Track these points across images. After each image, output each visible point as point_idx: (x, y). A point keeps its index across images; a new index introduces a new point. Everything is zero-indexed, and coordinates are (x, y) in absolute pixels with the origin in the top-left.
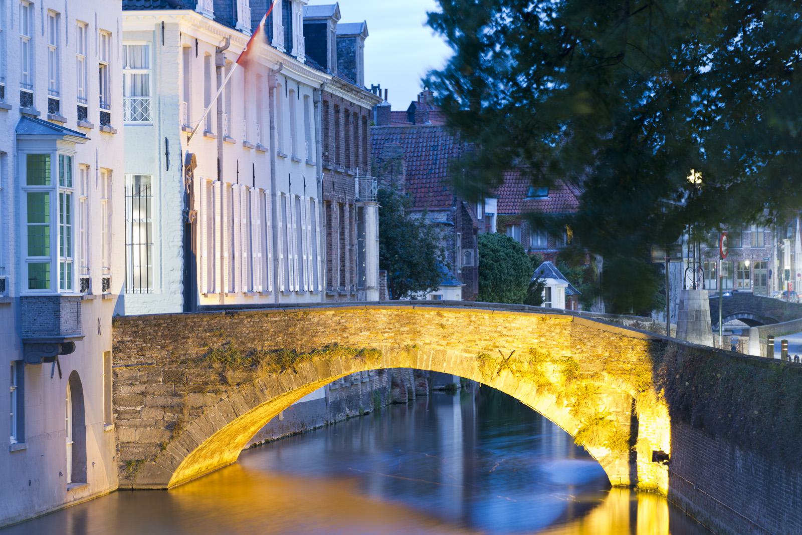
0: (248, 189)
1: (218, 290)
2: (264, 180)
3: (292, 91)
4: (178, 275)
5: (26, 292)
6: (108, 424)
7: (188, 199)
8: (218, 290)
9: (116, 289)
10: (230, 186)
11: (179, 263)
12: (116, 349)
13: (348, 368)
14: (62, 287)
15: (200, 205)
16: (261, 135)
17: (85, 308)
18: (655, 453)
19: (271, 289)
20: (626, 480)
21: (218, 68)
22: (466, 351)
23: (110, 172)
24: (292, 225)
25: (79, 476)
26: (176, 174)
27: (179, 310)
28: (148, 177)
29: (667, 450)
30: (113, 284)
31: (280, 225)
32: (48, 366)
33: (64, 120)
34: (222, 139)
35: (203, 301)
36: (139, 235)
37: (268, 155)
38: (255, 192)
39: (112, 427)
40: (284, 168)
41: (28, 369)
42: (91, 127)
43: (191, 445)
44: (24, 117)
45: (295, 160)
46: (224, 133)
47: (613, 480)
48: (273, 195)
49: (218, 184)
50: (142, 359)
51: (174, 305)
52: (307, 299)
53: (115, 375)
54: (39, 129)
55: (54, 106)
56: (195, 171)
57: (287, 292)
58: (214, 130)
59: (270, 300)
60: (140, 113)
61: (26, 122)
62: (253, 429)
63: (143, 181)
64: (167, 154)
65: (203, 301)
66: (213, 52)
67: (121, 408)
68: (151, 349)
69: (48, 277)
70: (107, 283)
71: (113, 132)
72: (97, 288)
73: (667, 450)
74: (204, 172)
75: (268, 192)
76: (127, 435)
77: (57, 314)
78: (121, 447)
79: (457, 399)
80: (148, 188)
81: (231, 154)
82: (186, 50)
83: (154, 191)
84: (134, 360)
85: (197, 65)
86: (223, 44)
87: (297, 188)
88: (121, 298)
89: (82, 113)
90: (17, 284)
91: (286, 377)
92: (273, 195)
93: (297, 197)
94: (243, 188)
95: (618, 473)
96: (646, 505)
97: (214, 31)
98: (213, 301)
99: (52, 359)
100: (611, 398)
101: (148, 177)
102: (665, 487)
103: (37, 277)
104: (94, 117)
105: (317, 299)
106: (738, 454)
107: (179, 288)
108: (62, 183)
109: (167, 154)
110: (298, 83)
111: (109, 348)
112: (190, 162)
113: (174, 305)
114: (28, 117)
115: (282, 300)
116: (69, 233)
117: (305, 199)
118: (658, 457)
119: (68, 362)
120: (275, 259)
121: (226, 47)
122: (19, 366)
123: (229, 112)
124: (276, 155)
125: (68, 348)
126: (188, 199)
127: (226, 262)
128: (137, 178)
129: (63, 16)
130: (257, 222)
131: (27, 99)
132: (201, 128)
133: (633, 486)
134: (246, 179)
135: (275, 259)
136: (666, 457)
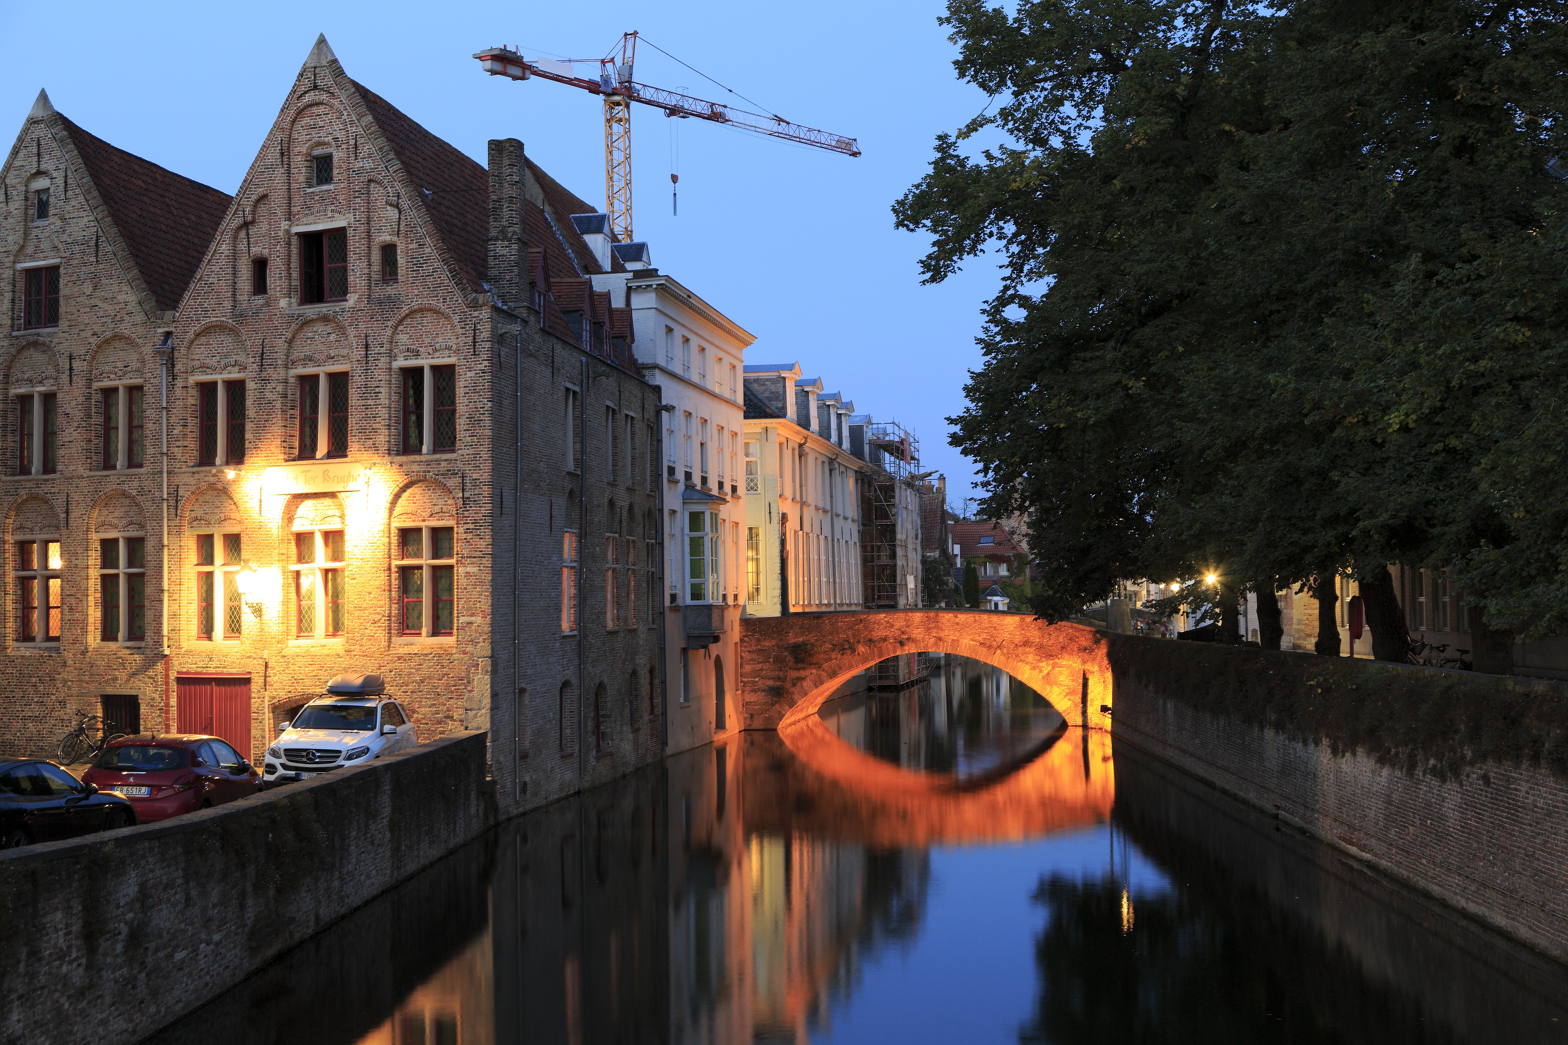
0: (818, 536)
1: (801, 603)
2: (827, 531)
3: (842, 472)
4: (778, 592)
5: (689, 601)
6: (737, 690)
7: (783, 543)
8: (801, 603)
9: (741, 601)
10: (807, 534)
11: (778, 584)
12: (742, 640)
13: (895, 652)
14: (713, 599)
15: (790, 547)
16: (824, 500)
17: (726, 613)
18: (1102, 706)
19: (832, 602)
20: (1080, 723)
21: (800, 457)
22: (972, 640)
23: (737, 524)
24: (844, 560)
25: (721, 724)
26: (776, 525)
27: (778, 614)
28: (757, 528)
29: (1110, 706)
30: (739, 597)
31: (837, 560)
32: (702, 651)
33: (710, 490)
34: (803, 504)
35: (792, 610)
36: (751, 566)
37: (829, 514)
38: (822, 538)
39: (739, 692)
40: (839, 523)
41: (691, 653)
42: (726, 494)
43: (792, 704)
44: (687, 487)
45: (846, 518)
46: (804, 500)
47: (1070, 722)
48: (833, 540)
49: (801, 533)
50: (759, 647)
51: (774, 611)
52: (853, 608)
53: (742, 657)
54: (697, 496)
55: (704, 480)
56: (787, 524)
57: (842, 605)
58: (798, 498)
59: (832, 609)
60: (752, 488)
61: (688, 491)
62: (827, 693)
63: (754, 531)
64: (770, 513)
65: (792, 610)
66: (797, 447)
67: (745, 680)
68: (765, 640)
69: (703, 592)
70: (736, 597)
71: (739, 498)
72: (730, 601)
73: (1110, 706)
74: (792, 524)
75: (830, 539)
76: (748, 698)
77: (710, 617)
78: (746, 704)
79: (943, 672)
80: (757, 535)
81: (808, 513)
82: (781, 444)
83: (761, 537)
84: (754, 648)
85: (788, 454)
86: (803, 442)
87: (847, 537)
88: (745, 606)
89: (721, 485)
90: (684, 597)
91: (847, 658)
92: (833, 540)
93: (847, 542)
94: (815, 535)
95: (1074, 718)
96: (1094, 740)
97: (798, 433)
98: (799, 610)
99: (705, 647)
100: (1069, 671)
101: (757, 528)
102: (1109, 728)
103: (697, 593)
104: (727, 488)
105: (859, 608)
106: (1169, 706)
107: (778, 600)
108: (712, 531)
109: (770, 513)
110: (846, 467)
111: (738, 640)
112: (784, 518)
113: (774, 611)
114: (690, 487)
115: (838, 609)
116: (716, 564)
117: (851, 543)
118: (1104, 709)
119: (715, 649)
120: (834, 583)
121: (804, 444)
122: (684, 650)
123: (806, 486)
124: (835, 515)
125: (716, 639)
126: (783, 543)
127: (806, 583)
128: (750, 529)
129: (709, 422)
130: (823, 558)
131: (688, 476)
132: (790, 497)
133: (1085, 726)
134: (817, 530)
135: (834, 583)
136: (1109, 709)
